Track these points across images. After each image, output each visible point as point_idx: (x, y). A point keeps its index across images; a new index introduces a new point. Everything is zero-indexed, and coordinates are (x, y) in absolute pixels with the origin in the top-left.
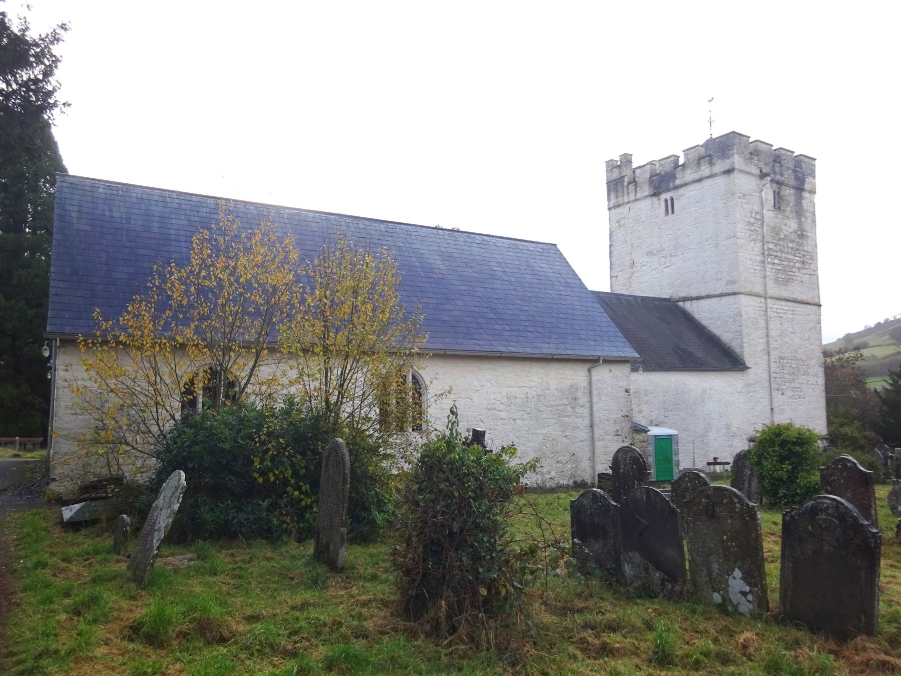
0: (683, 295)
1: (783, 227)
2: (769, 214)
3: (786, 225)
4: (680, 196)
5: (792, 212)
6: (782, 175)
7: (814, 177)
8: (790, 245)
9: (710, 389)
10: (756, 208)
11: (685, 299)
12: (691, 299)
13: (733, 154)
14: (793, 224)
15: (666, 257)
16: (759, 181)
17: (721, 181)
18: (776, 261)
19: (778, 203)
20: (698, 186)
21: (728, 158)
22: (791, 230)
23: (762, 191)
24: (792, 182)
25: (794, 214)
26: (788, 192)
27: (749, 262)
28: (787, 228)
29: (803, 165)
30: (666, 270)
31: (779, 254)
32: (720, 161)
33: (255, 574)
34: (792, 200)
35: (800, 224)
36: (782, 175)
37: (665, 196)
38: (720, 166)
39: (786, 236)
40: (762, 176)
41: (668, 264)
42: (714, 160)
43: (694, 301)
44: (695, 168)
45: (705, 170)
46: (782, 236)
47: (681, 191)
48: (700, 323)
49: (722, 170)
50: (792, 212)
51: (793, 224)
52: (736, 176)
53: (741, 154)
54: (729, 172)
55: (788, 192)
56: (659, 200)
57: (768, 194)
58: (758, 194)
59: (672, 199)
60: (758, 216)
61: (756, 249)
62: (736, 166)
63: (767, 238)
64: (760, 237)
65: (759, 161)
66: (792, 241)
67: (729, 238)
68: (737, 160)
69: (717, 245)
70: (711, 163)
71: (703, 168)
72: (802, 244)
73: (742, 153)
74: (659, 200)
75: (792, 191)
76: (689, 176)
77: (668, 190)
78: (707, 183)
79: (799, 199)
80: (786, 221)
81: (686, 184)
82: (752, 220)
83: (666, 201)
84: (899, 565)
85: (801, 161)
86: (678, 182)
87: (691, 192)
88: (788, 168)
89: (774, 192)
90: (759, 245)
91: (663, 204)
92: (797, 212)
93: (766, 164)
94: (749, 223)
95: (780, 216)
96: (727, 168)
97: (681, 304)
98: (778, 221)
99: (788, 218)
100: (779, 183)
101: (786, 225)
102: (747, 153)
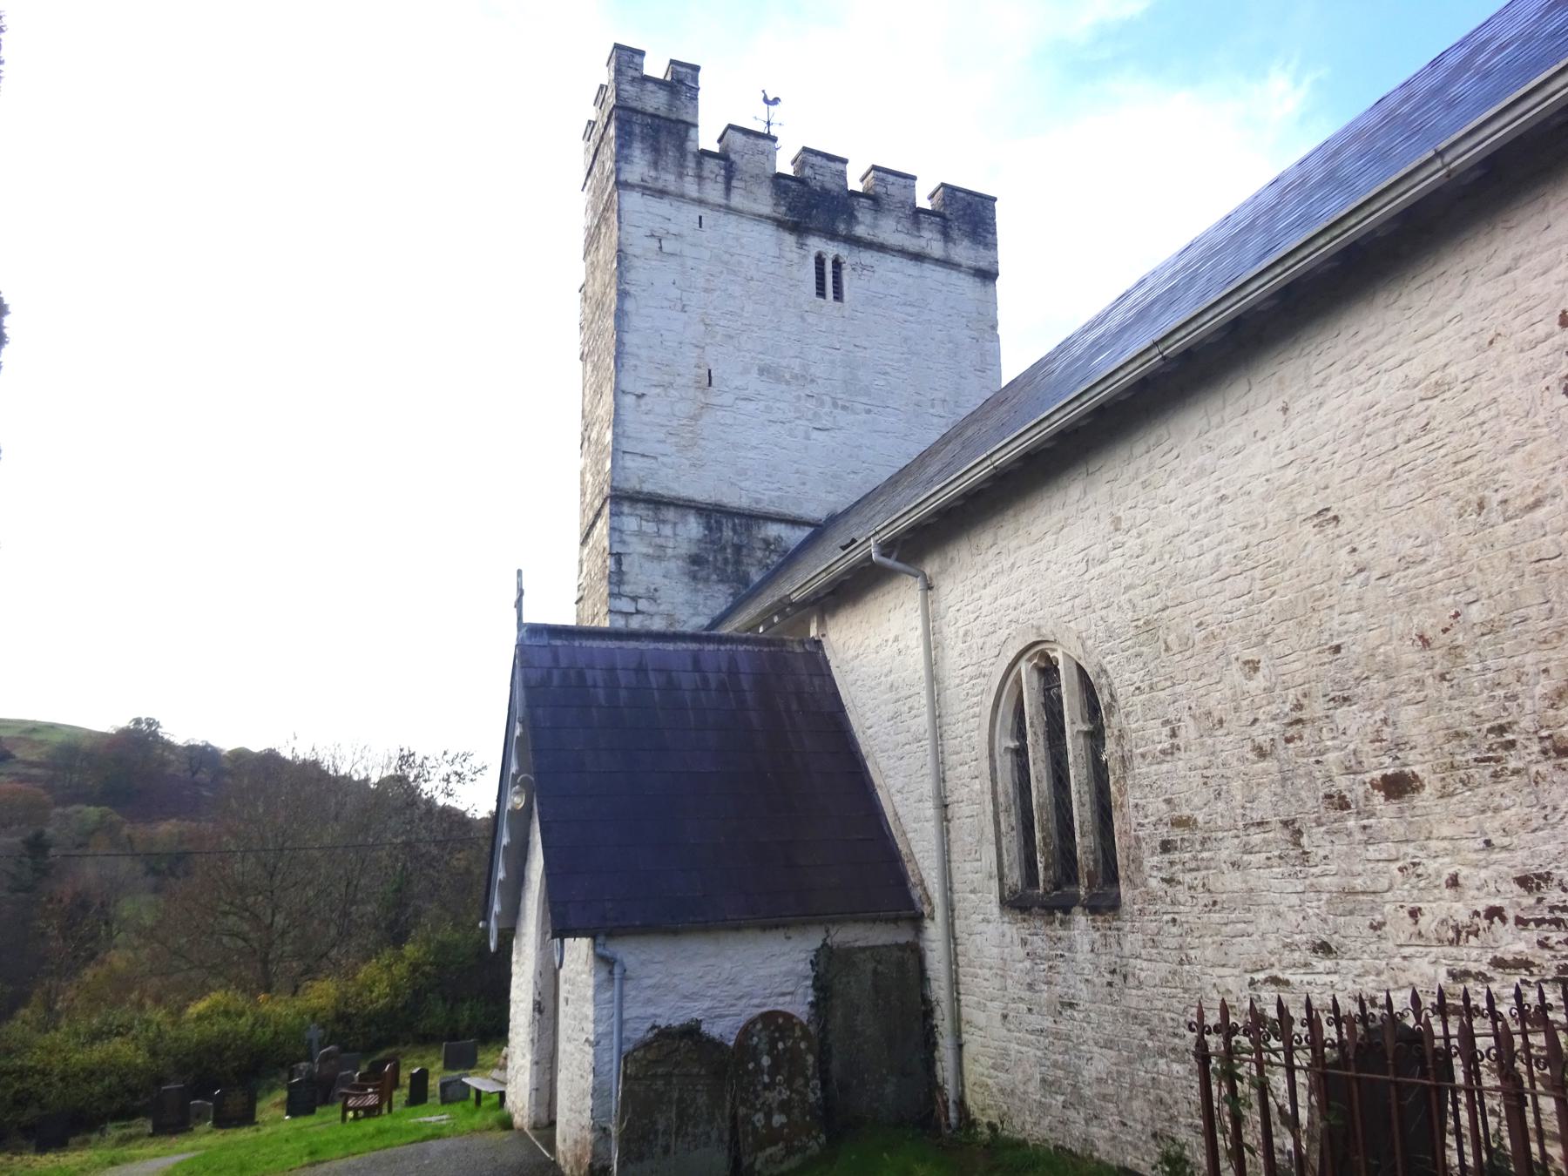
20: (910, 267)
32: (966, 243)
42: (955, 234)
59: (837, 264)
70: (946, 236)
71: (927, 234)
76: (889, 230)
77: (832, 235)
81: (882, 248)
83: (820, 261)
86: (860, 231)
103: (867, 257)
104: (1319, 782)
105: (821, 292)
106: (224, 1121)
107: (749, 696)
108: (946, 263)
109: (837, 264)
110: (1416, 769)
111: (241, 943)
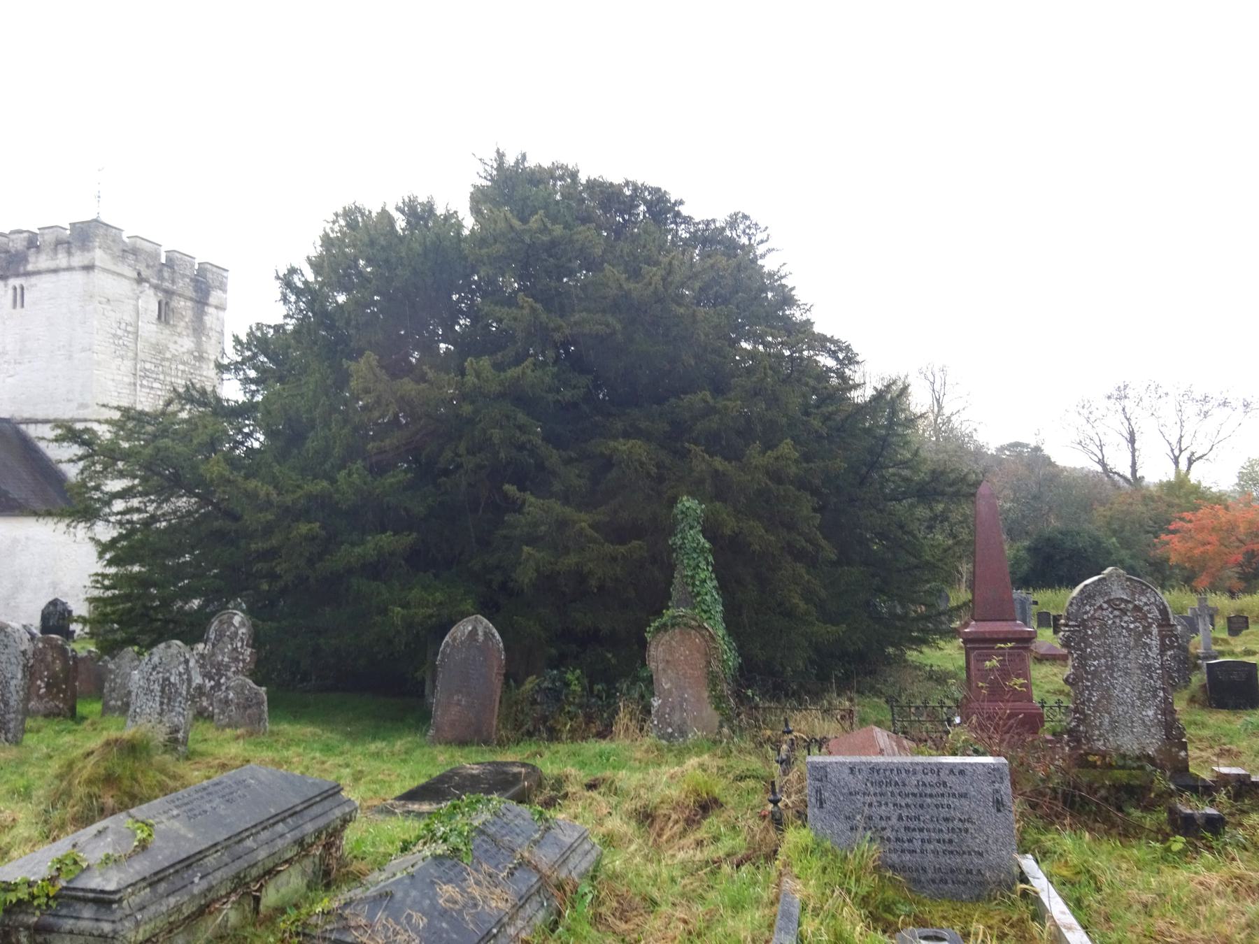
0: (26, 415)
1: (171, 345)
2: (149, 328)
3: (176, 342)
4: (32, 286)
5: (187, 328)
6: (173, 282)
7: (225, 291)
8: (181, 367)
9: (27, 538)
10: (128, 318)
11: (29, 421)
12: (36, 422)
13: (94, 248)
14: (187, 343)
15: (9, 363)
16: (135, 286)
17: (79, 276)
18: (156, 385)
19: (165, 314)
20: (52, 277)
21: (88, 251)
22: (184, 350)
23: (138, 298)
24: (190, 292)
25: (190, 332)
26: (183, 305)
27: (110, 383)
28: (177, 347)
29: (209, 275)
30: (9, 380)
31: (161, 377)
32: (79, 253)
33: (1139, 929)
34: (189, 315)
35: (199, 344)
36: (173, 282)
37: (14, 282)
38: (78, 259)
39: (174, 356)
40: (140, 280)
41: (12, 373)
42: (73, 251)
43: (40, 425)
44: (51, 254)
45: (62, 260)
46: (168, 355)
47: (33, 280)
48: (44, 454)
49: (81, 264)
50: (187, 328)
51: (187, 343)
52: (97, 276)
53: (107, 249)
54: (89, 268)
55: (181, 304)
56: (6, 286)
57: (150, 302)
58: (133, 302)
59: (22, 288)
60: (129, 329)
61: (122, 368)
62: (97, 263)
63: (141, 355)
64: (131, 354)
65: (136, 260)
66: (184, 363)
67: (83, 350)
68: (99, 256)
69: (70, 357)
70: (69, 253)
71: (60, 256)
72: (200, 367)
73: (109, 248)
74: (6, 286)
75: (189, 304)
76: (43, 262)
77: (17, 275)
78: (64, 276)
79: (199, 315)
80: (176, 338)
81: (38, 273)
82: (120, 332)
83: (15, 289)
84: (1237, 746)
85: (206, 270)
86: (30, 267)
87: (45, 282)
88: (184, 276)
89: (160, 303)
90: (129, 364)
91: (11, 292)
92: (195, 330)
93: (148, 266)
94: (115, 335)
95: (167, 332)
96: (86, 262)
97: (23, 427)
98: (161, 337)
99: (180, 335)
100: (169, 293)
101: (176, 342)
102: (117, 250)
103: (34, 280)
104: (1012, 817)
105: (15, 306)
106: (601, 735)
107: (190, 835)
108: (69, 269)
109: (22, 288)
110: (674, 593)
111: (1171, 527)
